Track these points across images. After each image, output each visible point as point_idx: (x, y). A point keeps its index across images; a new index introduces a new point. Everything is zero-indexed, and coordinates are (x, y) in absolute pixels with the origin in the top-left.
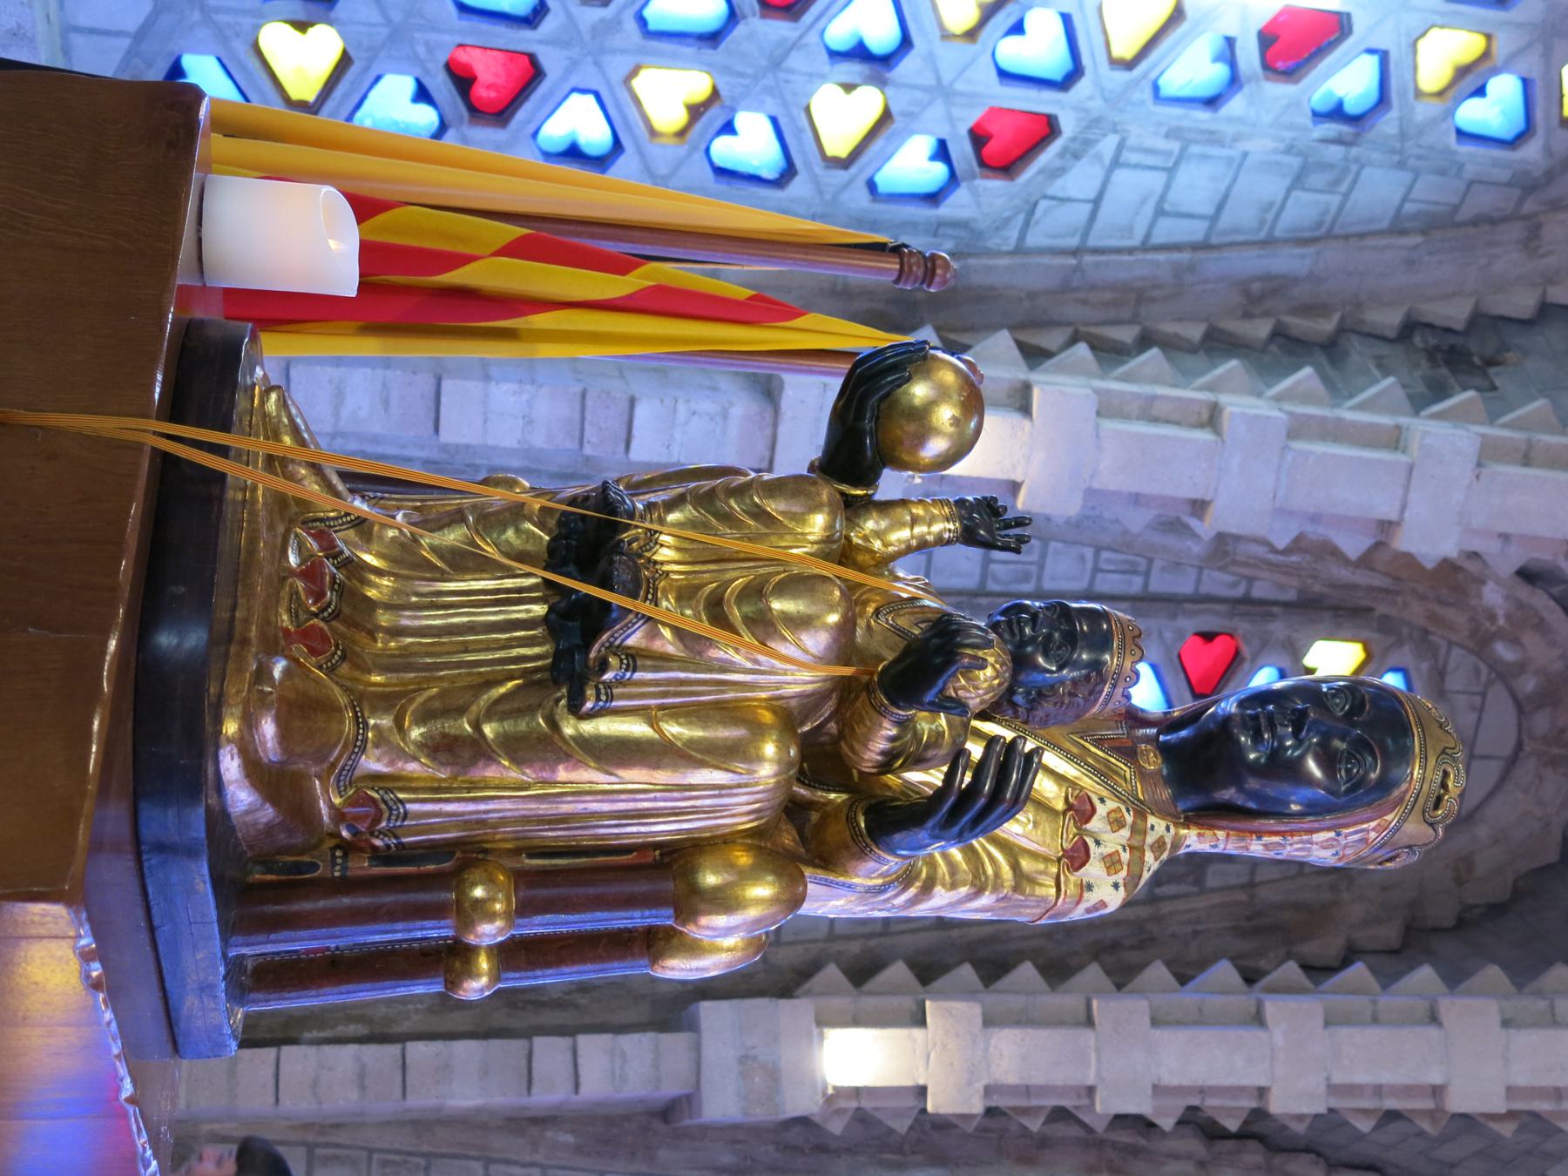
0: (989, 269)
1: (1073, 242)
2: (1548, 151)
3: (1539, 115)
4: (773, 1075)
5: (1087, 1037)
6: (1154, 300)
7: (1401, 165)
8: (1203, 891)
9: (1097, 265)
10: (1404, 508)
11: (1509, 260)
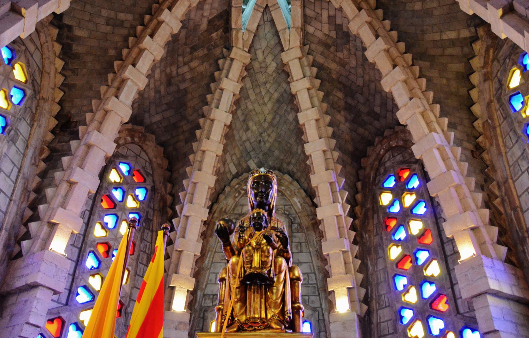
0: (7, 223)
1: (8, 199)
2: (29, 89)
3: (22, 87)
4: (180, 323)
5: (185, 252)
6: (27, 186)
7: (20, 120)
8: (153, 220)
9: (16, 196)
10: (104, 151)
11: (46, 106)
